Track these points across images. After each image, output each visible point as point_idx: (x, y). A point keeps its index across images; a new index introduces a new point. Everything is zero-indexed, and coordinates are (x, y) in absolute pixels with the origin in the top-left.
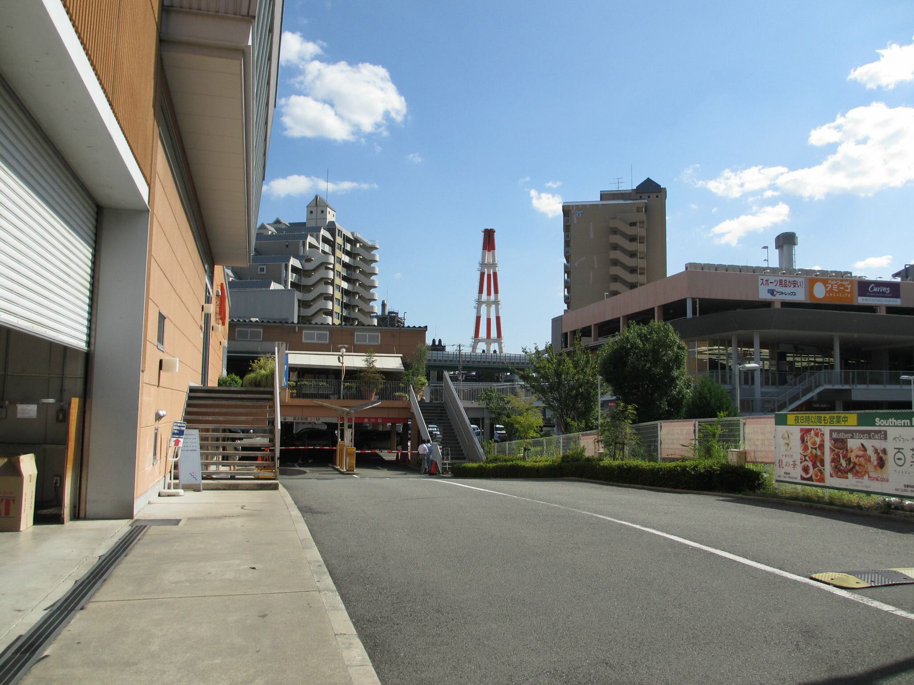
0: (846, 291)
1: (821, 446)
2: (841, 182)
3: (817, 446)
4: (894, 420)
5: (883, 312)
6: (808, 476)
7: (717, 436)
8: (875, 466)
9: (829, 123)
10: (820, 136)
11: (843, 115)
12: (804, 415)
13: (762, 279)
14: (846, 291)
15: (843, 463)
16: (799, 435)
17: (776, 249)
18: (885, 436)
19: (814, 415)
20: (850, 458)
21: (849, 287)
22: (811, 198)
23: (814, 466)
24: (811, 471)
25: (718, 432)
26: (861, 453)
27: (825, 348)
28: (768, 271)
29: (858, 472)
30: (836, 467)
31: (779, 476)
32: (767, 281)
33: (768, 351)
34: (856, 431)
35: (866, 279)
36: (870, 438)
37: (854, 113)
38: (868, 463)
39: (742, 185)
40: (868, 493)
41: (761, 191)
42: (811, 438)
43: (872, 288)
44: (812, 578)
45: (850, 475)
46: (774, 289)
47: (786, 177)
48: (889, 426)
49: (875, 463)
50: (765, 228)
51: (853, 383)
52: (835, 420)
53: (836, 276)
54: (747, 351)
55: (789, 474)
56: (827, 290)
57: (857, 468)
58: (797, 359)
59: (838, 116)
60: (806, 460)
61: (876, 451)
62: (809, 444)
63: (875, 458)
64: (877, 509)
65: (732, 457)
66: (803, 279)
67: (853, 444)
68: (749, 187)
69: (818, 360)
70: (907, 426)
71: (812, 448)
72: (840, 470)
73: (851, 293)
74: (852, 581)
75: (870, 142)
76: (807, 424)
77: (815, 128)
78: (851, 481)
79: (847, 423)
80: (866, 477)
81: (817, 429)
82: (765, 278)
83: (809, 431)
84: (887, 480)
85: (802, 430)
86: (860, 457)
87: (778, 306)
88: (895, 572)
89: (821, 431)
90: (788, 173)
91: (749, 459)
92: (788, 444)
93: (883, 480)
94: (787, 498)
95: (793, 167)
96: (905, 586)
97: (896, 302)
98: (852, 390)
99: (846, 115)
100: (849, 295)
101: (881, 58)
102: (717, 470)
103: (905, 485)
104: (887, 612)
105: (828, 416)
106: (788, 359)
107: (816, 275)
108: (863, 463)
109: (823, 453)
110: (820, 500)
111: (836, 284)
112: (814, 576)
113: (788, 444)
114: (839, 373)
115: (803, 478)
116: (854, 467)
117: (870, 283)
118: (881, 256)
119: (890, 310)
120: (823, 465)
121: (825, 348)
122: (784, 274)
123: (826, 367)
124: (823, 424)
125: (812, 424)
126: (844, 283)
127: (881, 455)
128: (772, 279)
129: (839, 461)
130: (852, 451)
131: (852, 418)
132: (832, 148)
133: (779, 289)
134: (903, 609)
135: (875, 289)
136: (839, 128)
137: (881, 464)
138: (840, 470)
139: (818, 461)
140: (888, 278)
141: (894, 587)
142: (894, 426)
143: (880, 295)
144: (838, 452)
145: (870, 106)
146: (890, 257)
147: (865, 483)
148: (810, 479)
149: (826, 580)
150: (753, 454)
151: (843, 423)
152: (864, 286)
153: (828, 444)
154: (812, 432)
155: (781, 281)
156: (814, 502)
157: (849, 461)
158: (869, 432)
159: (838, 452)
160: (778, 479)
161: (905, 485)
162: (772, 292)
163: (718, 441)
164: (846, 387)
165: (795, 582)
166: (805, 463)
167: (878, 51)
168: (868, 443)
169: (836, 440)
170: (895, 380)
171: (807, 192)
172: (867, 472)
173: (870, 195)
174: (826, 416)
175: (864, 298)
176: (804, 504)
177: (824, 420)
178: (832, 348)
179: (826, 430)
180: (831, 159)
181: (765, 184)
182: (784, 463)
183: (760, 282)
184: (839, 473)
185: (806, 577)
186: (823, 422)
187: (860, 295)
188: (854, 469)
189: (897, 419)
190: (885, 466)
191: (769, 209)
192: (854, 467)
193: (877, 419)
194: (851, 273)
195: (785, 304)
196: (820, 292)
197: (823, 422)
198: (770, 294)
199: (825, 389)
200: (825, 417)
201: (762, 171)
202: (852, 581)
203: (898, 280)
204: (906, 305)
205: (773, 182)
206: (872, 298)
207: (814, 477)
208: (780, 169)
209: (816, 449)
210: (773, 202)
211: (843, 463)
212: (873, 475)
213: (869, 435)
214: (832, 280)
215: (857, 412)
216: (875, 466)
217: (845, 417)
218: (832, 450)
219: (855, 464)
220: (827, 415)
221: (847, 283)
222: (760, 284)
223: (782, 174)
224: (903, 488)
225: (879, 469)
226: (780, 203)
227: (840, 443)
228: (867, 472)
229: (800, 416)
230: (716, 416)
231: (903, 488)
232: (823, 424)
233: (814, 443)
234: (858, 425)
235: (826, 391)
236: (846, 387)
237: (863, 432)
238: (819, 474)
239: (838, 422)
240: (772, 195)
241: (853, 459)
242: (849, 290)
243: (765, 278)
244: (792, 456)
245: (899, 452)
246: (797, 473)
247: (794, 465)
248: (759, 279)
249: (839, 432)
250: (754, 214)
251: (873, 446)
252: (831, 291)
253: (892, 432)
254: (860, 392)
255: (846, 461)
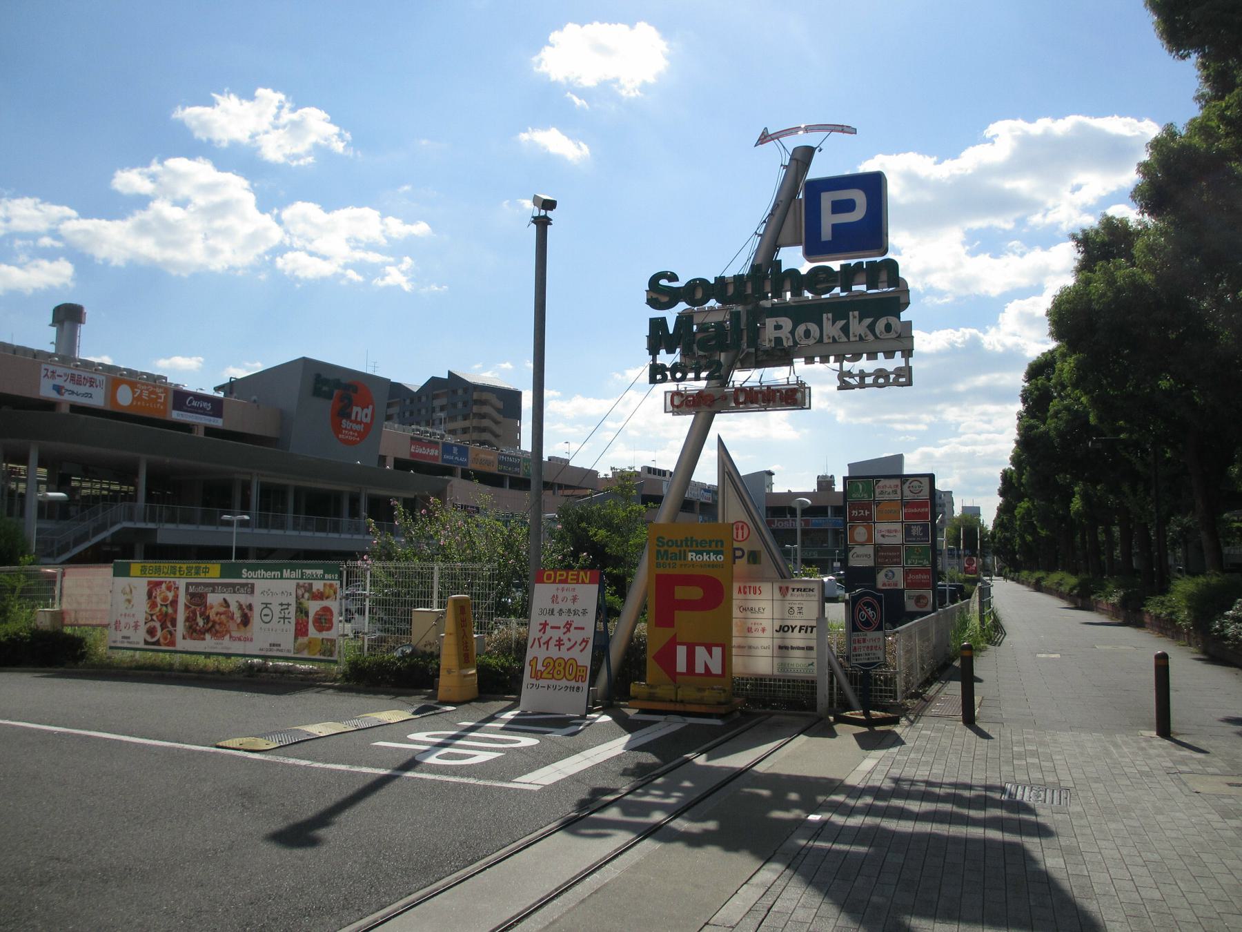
0: (159, 400)
1: (174, 603)
2: (147, 247)
3: (168, 602)
4: (263, 572)
5: (200, 434)
6: (155, 639)
7: (18, 591)
8: (238, 625)
9: (141, 167)
10: (131, 180)
11: (161, 162)
12: (154, 565)
13: (47, 370)
14: (159, 400)
15: (201, 622)
16: (145, 589)
17: (52, 325)
18: (251, 589)
19: (167, 565)
20: (209, 616)
21: (163, 395)
22: (106, 262)
23: (163, 627)
24: (159, 634)
25: (19, 586)
26: (222, 609)
27: (125, 473)
28: (57, 359)
29: (217, 632)
30: (190, 627)
31: (115, 642)
32: (53, 372)
33: (46, 470)
34: (218, 584)
35: (184, 388)
36: (234, 592)
37: (179, 164)
38: (231, 621)
39: (7, 220)
40: (228, 656)
41: (35, 236)
42: (159, 594)
43: (191, 402)
44: (218, 747)
45: (208, 636)
46: (61, 384)
47: (76, 226)
48: (258, 578)
49: (239, 620)
50: (35, 290)
51: (160, 521)
52: (193, 571)
53: (147, 379)
54: (16, 468)
55: (129, 638)
56: (136, 396)
57: (217, 627)
58: (84, 484)
59: (155, 161)
60: (152, 620)
61: (240, 607)
62: (159, 600)
63: (239, 615)
64: (239, 673)
65: (42, 617)
66: (104, 378)
67: (214, 599)
68: (17, 224)
69: (113, 487)
70: (278, 578)
71: (161, 605)
72: (195, 631)
73: (164, 404)
74: (262, 744)
75: (191, 208)
76: (157, 575)
77: (122, 169)
78: (209, 643)
79: (207, 575)
80: (227, 637)
81: (170, 582)
82: (51, 368)
83: (159, 584)
84: (251, 640)
85: (149, 583)
86: (221, 614)
87: (65, 409)
88: (298, 730)
89: (175, 584)
90: (77, 219)
91: (67, 621)
92: (129, 601)
93: (246, 639)
94: (130, 668)
95: (85, 214)
96: (310, 742)
97: (218, 423)
98: (158, 531)
99: (166, 163)
100: (162, 407)
101: (216, 105)
102: (25, 637)
103: (270, 645)
104: (305, 766)
105: (184, 566)
106: (73, 484)
107: (122, 375)
108: (225, 621)
109: (175, 611)
110: (171, 667)
111: (147, 390)
112: (220, 744)
113: (129, 601)
114: (143, 507)
115: (146, 642)
116: (213, 626)
117: (188, 394)
118: (190, 357)
119: (210, 431)
120: (174, 625)
121: (125, 473)
122: (77, 366)
123: (124, 499)
124: (178, 575)
125: (164, 575)
126: (158, 390)
127: (246, 611)
128: (60, 371)
129: (196, 620)
130: (211, 608)
131: (214, 570)
132: (143, 202)
133: (69, 386)
134: (318, 761)
135: (194, 404)
136: (153, 178)
137: (246, 621)
138: (195, 631)
139: (167, 620)
140: (209, 391)
141: (301, 744)
142: (263, 578)
143: (199, 411)
144: (195, 610)
145: (194, 160)
146: (201, 359)
147: (226, 645)
148: (157, 643)
149: (234, 746)
150: (73, 615)
151: (203, 575)
152: (181, 398)
153: (182, 600)
154: (164, 586)
155: (73, 376)
156: (164, 670)
157: (207, 619)
158: (233, 585)
159: (195, 610)
160: (113, 645)
161: (270, 645)
162: (58, 389)
163: (19, 597)
164: (151, 526)
165: (202, 752)
166: (152, 624)
167: (214, 95)
168: (233, 599)
169: (193, 595)
170: (209, 519)
171: (101, 253)
172: (228, 632)
173: (185, 275)
174: (182, 565)
175: (180, 413)
176: (153, 673)
177: (180, 571)
178: (136, 473)
179: (182, 583)
180: (140, 216)
181: (43, 226)
182: (123, 625)
183: (44, 373)
184: (194, 634)
185: (211, 746)
186: (178, 573)
187: (175, 408)
188: (213, 628)
189: (266, 571)
190: (250, 624)
191: (45, 264)
192: (213, 626)
193: (244, 571)
194: (166, 378)
195: (75, 408)
196: (125, 397)
197: (178, 573)
198: (55, 392)
199: (124, 528)
200: (180, 568)
201: (41, 207)
202: (262, 744)
203: (221, 395)
204: (228, 428)
205: (54, 227)
206: (189, 414)
207: (162, 640)
208: (67, 211)
209: (166, 606)
210: (51, 255)
211: (201, 622)
212: (234, 634)
213: (234, 588)
214: (143, 384)
215: (221, 561)
216: (238, 625)
217: (206, 568)
218: (187, 607)
219: (214, 622)
220: (184, 565)
221: (161, 390)
222: (42, 375)
223: (69, 218)
224: (269, 647)
225: (241, 626)
226: (62, 259)
227: (197, 598)
228: (228, 632)
229: (149, 565)
230: (17, 563)
231: (269, 647)
232: (178, 575)
233: (165, 599)
234: (222, 577)
235: (125, 531)
236: (151, 526)
237: (226, 585)
238: (169, 636)
239: (197, 573)
240: (52, 246)
241: (212, 616)
242: (162, 400)
243: (51, 368)
244: (134, 615)
245: (266, 607)
246: (139, 637)
247: (136, 627)
248: (43, 370)
249: (197, 585)
250: (21, 266)
251: (237, 602)
252: (139, 398)
253: (260, 585)
254: (169, 533)
255: (203, 619)
